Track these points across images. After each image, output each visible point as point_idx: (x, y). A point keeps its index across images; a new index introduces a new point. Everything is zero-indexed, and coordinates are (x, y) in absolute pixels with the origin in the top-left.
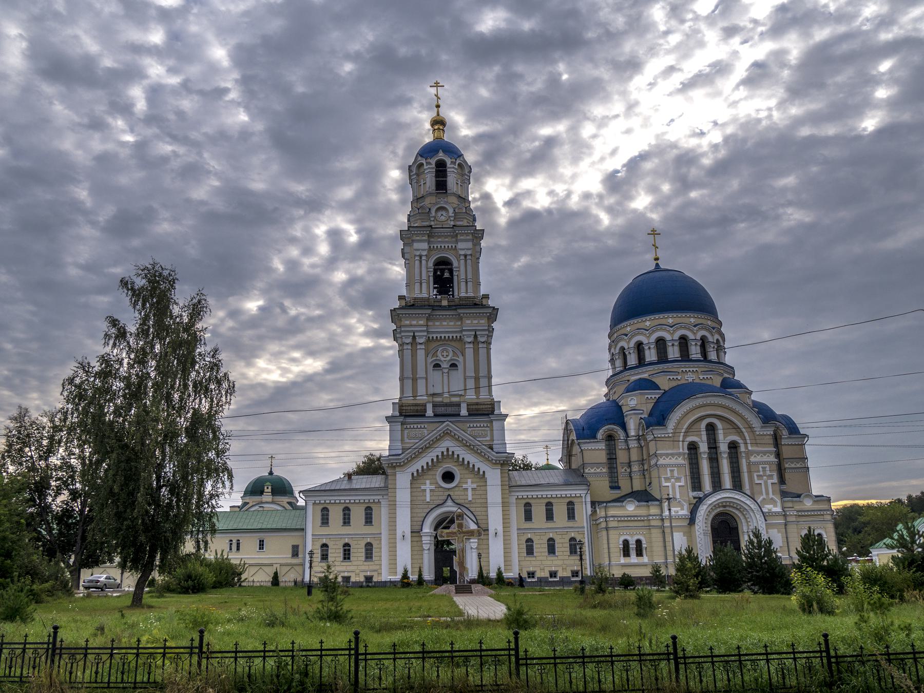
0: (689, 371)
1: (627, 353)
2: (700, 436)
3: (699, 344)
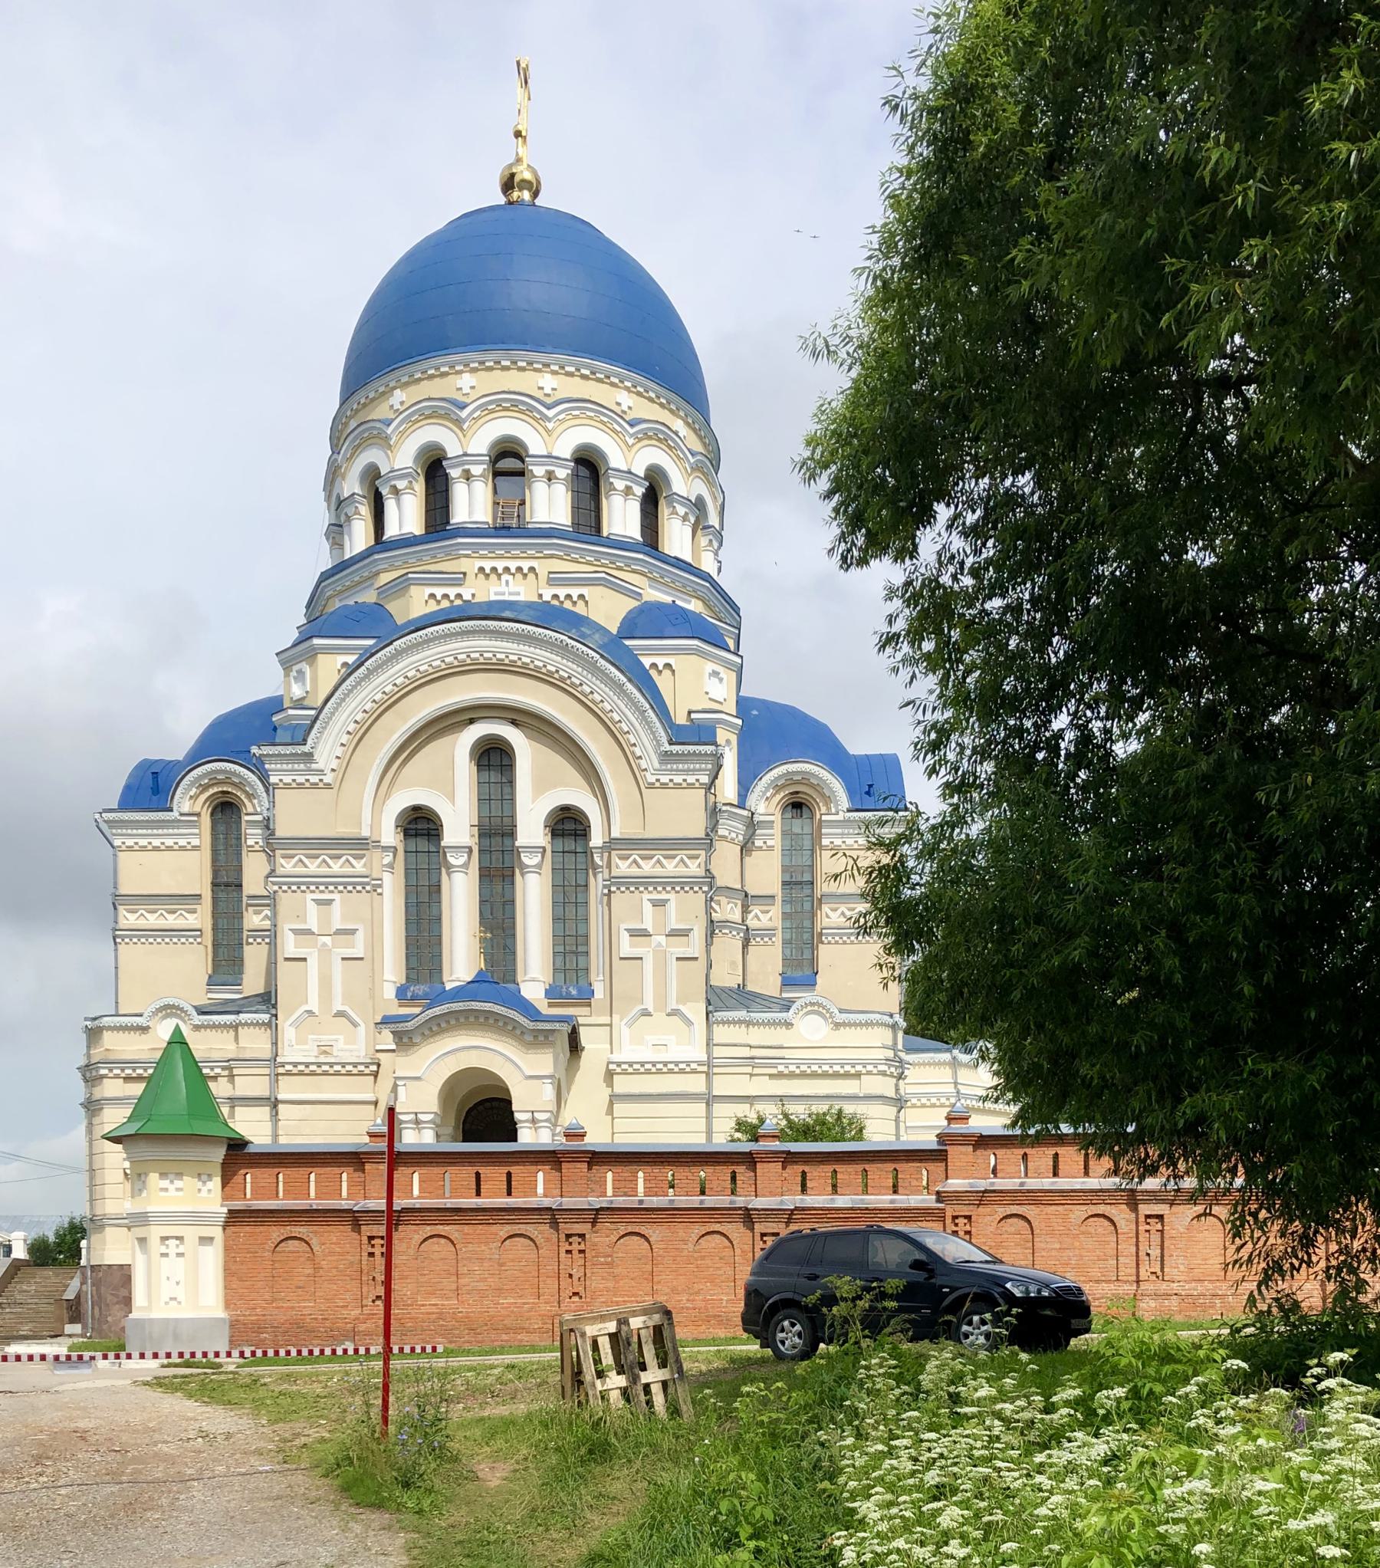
0: (507, 570)
1: (384, 491)
2: (452, 797)
3: (639, 491)
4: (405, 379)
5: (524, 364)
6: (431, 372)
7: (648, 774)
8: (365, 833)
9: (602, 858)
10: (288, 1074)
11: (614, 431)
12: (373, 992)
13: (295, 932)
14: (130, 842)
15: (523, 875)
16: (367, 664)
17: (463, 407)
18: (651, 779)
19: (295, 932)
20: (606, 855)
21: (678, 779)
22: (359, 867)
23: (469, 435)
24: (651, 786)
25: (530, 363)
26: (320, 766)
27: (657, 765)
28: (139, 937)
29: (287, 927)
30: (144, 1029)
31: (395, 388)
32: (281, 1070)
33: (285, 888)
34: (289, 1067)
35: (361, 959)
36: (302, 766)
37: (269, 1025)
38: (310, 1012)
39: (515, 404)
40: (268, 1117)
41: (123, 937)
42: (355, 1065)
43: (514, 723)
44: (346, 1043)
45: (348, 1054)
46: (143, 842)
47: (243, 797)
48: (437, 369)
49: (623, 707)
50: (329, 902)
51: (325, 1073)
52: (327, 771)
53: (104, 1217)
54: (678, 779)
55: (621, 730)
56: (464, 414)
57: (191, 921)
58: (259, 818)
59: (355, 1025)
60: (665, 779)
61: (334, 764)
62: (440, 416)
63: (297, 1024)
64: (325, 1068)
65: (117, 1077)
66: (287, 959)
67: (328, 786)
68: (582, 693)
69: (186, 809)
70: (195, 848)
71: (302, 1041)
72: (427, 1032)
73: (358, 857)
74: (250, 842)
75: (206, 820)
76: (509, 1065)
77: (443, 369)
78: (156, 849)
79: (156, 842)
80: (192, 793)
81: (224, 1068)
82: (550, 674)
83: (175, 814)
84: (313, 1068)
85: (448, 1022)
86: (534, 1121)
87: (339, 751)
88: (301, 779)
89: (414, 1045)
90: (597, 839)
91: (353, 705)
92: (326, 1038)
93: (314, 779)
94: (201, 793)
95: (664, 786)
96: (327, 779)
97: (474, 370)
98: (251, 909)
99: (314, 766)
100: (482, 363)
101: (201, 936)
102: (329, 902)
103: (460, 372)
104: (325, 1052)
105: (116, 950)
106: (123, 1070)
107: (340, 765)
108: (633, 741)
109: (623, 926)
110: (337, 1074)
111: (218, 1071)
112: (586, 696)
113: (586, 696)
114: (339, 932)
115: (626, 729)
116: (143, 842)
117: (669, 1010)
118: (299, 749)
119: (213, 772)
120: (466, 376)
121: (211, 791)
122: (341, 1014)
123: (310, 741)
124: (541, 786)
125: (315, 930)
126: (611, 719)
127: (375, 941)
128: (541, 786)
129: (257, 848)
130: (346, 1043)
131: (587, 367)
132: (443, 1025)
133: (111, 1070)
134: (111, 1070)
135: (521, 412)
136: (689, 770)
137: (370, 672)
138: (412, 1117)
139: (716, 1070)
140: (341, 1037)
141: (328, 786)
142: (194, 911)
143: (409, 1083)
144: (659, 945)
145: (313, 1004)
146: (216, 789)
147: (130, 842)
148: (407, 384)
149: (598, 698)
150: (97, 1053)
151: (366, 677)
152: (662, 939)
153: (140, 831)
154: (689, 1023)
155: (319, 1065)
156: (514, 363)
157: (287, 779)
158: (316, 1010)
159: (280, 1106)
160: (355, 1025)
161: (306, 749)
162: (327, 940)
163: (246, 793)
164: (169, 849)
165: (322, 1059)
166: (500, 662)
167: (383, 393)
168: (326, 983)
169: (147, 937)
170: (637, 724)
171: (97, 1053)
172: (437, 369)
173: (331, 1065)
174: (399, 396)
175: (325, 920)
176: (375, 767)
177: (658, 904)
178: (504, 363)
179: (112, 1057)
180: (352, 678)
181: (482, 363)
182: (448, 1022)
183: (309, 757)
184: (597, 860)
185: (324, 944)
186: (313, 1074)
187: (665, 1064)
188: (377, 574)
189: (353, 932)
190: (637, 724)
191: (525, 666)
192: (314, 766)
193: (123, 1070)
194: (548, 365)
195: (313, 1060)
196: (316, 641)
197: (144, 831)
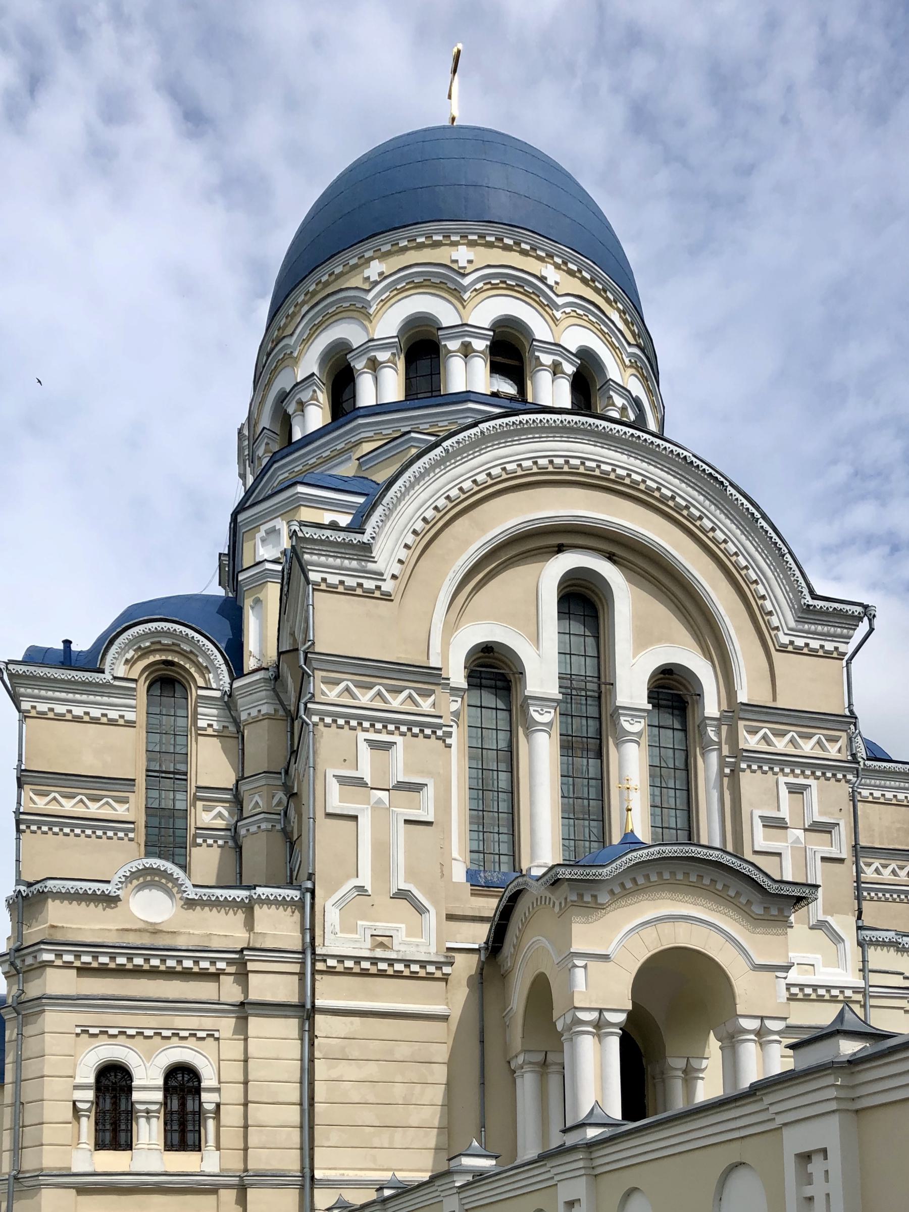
2: (536, 639)
4: (386, 248)
5: (528, 247)
6: (420, 240)
7: (780, 634)
8: (434, 662)
9: (718, 733)
10: (331, 971)
11: (612, 345)
12: (444, 870)
13: (343, 781)
14: (43, 707)
15: (617, 745)
16: (446, 444)
17: (464, 275)
18: (785, 640)
19: (343, 781)
20: (724, 729)
21: (815, 644)
22: (426, 705)
23: (470, 306)
24: (783, 649)
25: (534, 249)
26: (378, 567)
27: (792, 624)
28: (51, 825)
29: (330, 772)
30: (111, 901)
31: (372, 259)
32: (320, 966)
33: (328, 720)
34: (331, 962)
35: (429, 824)
36: (354, 564)
37: (299, 905)
38: (361, 889)
39: (521, 283)
40: (295, 1033)
41: (29, 824)
42: (423, 964)
43: (611, 558)
44: (408, 935)
45: (414, 949)
46: (60, 709)
47: (192, 670)
48: (429, 237)
49: (752, 549)
50: (388, 746)
51: (382, 974)
52: (387, 576)
53: (40, 1173)
54: (815, 644)
55: (746, 579)
56: (466, 281)
57: (121, 811)
58: (217, 694)
59: (421, 909)
60: (800, 642)
61: (396, 569)
62: (434, 286)
63: (343, 905)
64: (383, 966)
65: (68, 966)
66: (329, 815)
67: (387, 597)
68: (701, 529)
69: (121, 671)
70: (130, 724)
71: (348, 927)
72: (617, 890)
73: (426, 694)
74: (202, 723)
75: (142, 687)
76: (729, 946)
77: (435, 238)
78: (77, 719)
79: (78, 711)
80: (129, 656)
81: (230, 962)
82: (663, 499)
83: (107, 676)
84: (365, 965)
85: (647, 877)
86: (761, 1033)
87: (403, 554)
88: (351, 582)
89: (600, 907)
90: (711, 707)
91: (424, 496)
92: (382, 927)
93: (369, 584)
94: (140, 658)
95: (798, 651)
96: (388, 586)
97: (472, 244)
98: (200, 804)
99: (371, 566)
100: (482, 236)
101: (133, 830)
102: (388, 746)
103: (455, 244)
104: (382, 945)
105: (18, 839)
106: (78, 956)
107: (403, 572)
108: (762, 592)
109: (757, 813)
110: (398, 975)
111: (221, 965)
112: (705, 532)
113: (705, 532)
114: (401, 786)
115: (754, 577)
116: (60, 709)
117: (813, 922)
118: (356, 538)
119: (158, 633)
120: (463, 249)
121: (152, 659)
122: (402, 895)
123: (369, 529)
124: (643, 640)
125: (368, 780)
126: (736, 565)
127: (443, 804)
128: (643, 640)
129: (210, 731)
130: (408, 935)
131: (589, 271)
132: (641, 881)
133: (59, 955)
134: (59, 955)
135: (526, 294)
136: (828, 635)
137: (449, 456)
138: (594, 1016)
139: (873, 1002)
140: (403, 926)
141: (387, 597)
142: (124, 801)
143: (593, 965)
144: (797, 840)
145: (365, 879)
146: (158, 657)
147: (43, 707)
148: (388, 254)
149: (720, 536)
150: (34, 932)
151: (440, 463)
152: (800, 833)
153: (57, 694)
154: (837, 938)
155: (374, 961)
156: (517, 243)
157: (333, 579)
158: (368, 887)
159: (319, 1018)
160: (421, 909)
161: (365, 538)
162: (384, 795)
163: (198, 666)
164: (95, 721)
165: (379, 953)
166: (605, 476)
167: (355, 267)
168: (382, 851)
169: (62, 826)
170: (769, 574)
171: (34, 932)
172: (429, 237)
173: (391, 962)
174: (375, 269)
175: (381, 769)
176: (447, 582)
177: (796, 790)
178: (506, 241)
179: (59, 937)
180: (425, 459)
181: (482, 236)
182: (647, 877)
183: (365, 551)
184: (711, 733)
185: (380, 801)
186: (365, 973)
187: (815, 988)
188: (359, 443)
189: (417, 788)
190: (769, 574)
191: (634, 485)
192: (371, 566)
193: (78, 956)
194: (550, 256)
195: (367, 954)
196: (301, 489)
197: (63, 695)
